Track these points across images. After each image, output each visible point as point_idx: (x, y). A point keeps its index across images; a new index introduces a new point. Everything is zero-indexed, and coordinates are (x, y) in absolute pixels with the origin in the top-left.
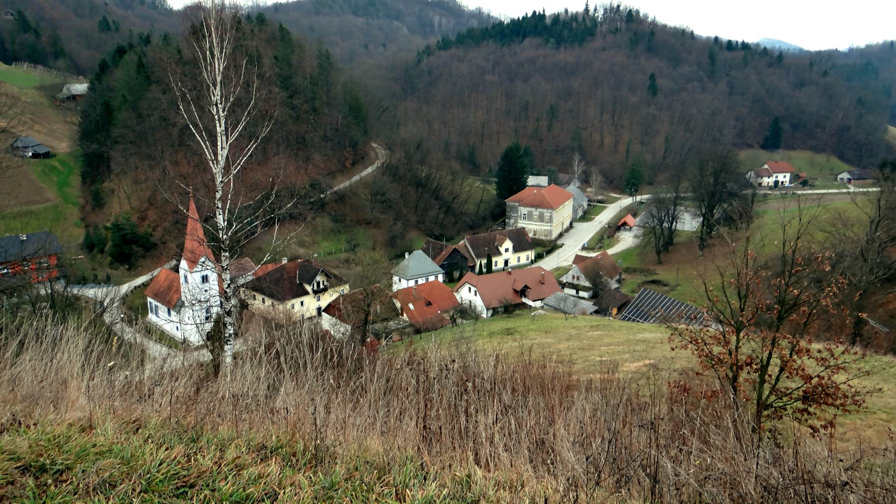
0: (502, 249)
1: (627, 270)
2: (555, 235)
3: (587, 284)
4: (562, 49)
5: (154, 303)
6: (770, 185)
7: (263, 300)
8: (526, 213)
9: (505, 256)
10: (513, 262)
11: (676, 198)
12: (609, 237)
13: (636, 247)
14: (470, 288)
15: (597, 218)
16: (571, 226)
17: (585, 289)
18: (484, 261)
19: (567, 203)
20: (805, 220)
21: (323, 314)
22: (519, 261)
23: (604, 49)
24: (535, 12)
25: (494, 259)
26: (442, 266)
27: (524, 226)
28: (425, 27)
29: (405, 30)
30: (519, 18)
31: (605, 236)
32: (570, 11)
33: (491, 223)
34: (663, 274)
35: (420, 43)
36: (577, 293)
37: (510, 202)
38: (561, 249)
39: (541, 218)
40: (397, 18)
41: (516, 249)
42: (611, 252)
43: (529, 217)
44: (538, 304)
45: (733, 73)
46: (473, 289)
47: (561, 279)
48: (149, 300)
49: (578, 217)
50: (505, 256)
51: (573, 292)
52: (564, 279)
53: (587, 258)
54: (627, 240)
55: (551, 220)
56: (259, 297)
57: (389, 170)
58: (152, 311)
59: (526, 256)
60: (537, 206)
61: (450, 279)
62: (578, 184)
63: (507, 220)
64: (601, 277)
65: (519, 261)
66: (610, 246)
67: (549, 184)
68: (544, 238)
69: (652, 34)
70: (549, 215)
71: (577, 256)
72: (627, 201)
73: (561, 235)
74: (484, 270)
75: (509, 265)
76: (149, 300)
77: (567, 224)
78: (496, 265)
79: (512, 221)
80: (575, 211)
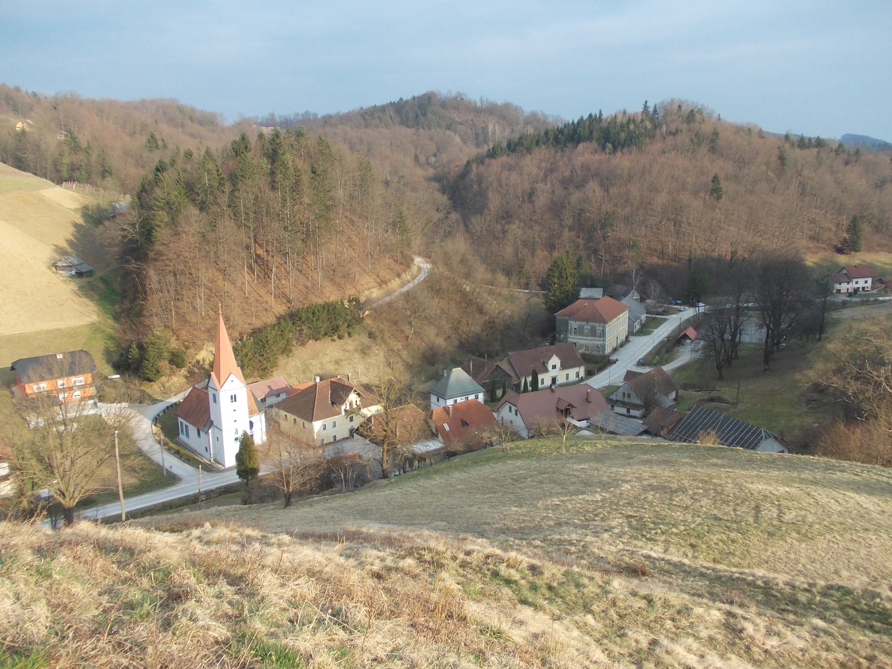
0: (550, 367)
1: (685, 387)
2: (608, 350)
3: (638, 402)
4: (619, 154)
5: (185, 423)
6: (850, 291)
7: (295, 420)
8: (576, 327)
9: (552, 373)
10: (561, 380)
11: (738, 308)
12: (667, 352)
13: (696, 361)
14: (510, 408)
15: (656, 331)
16: (627, 340)
17: (636, 407)
18: (529, 379)
19: (621, 315)
20: (83, 262)
21: (355, 434)
22: (567, 378)
23: (664, 152)
24: (590, 115)
25: (540, 377)
26: (483, 385)
27: (575, 341)
28: (479, 137)
29: (457, 139)
30: (76, 225)
31: (664, 350)
32: (628, 111)
33: (540, 339)
34: (726, 391)
35: (471, 151)
36: (628, 411)
37: (560, 315)
38: (614, 366)
39: (593, 333)
40: (448, 128)
41: (564, 366)
42: (667, 368)
43: (580, 331)
44: (584, 424)
45: (806, 172)
46: (513, 408)
47: (611, 397)
48: (180, 420)
49: (635, 331)
50: (552, 373)
51: (624, 411)
52: (614, 397)
53: (641, 374)
54: (685, 356)
55: (603, 334)
56: (291, 417)
57: (432, 285)
58: (182, 431)
59: (573, 374)
60: (587, 320)
61: (492, 399)
62: (637, 296)
63: (557, 335)
64: (655, 394)
65: (567, 378)
66: (667, 362)
67: (604, 295)
68: (596, 353)
69: (716, 134)
70: (601, 328)
71: (628, 372)
72: (688, 313)
73: (615, 350)
74: (530, 388)
75: (558, 383)
76: (180, 420)
77: (622, 337)
78: (542, 383)
79: (562, 336)
80: (631, 326)
